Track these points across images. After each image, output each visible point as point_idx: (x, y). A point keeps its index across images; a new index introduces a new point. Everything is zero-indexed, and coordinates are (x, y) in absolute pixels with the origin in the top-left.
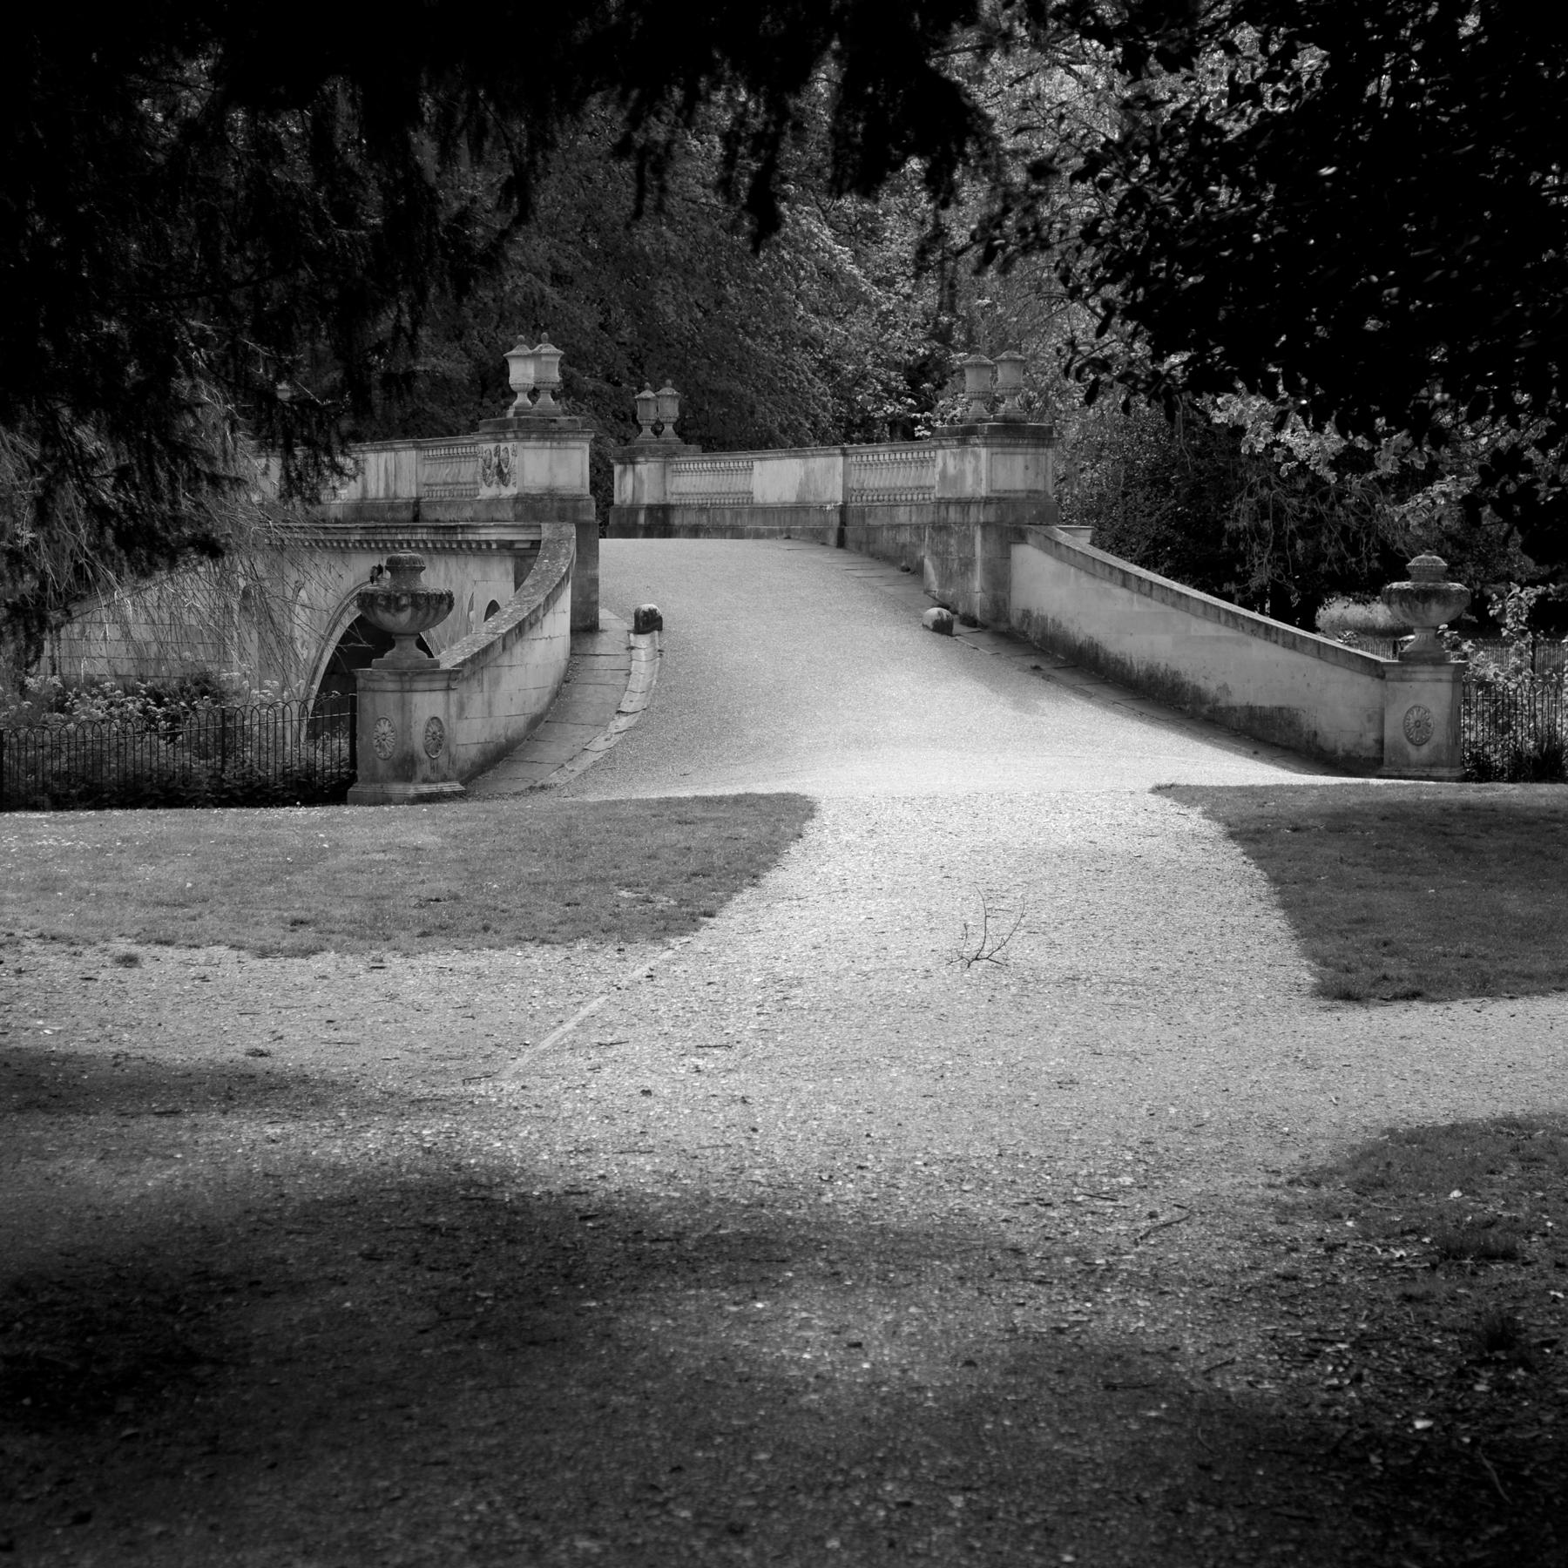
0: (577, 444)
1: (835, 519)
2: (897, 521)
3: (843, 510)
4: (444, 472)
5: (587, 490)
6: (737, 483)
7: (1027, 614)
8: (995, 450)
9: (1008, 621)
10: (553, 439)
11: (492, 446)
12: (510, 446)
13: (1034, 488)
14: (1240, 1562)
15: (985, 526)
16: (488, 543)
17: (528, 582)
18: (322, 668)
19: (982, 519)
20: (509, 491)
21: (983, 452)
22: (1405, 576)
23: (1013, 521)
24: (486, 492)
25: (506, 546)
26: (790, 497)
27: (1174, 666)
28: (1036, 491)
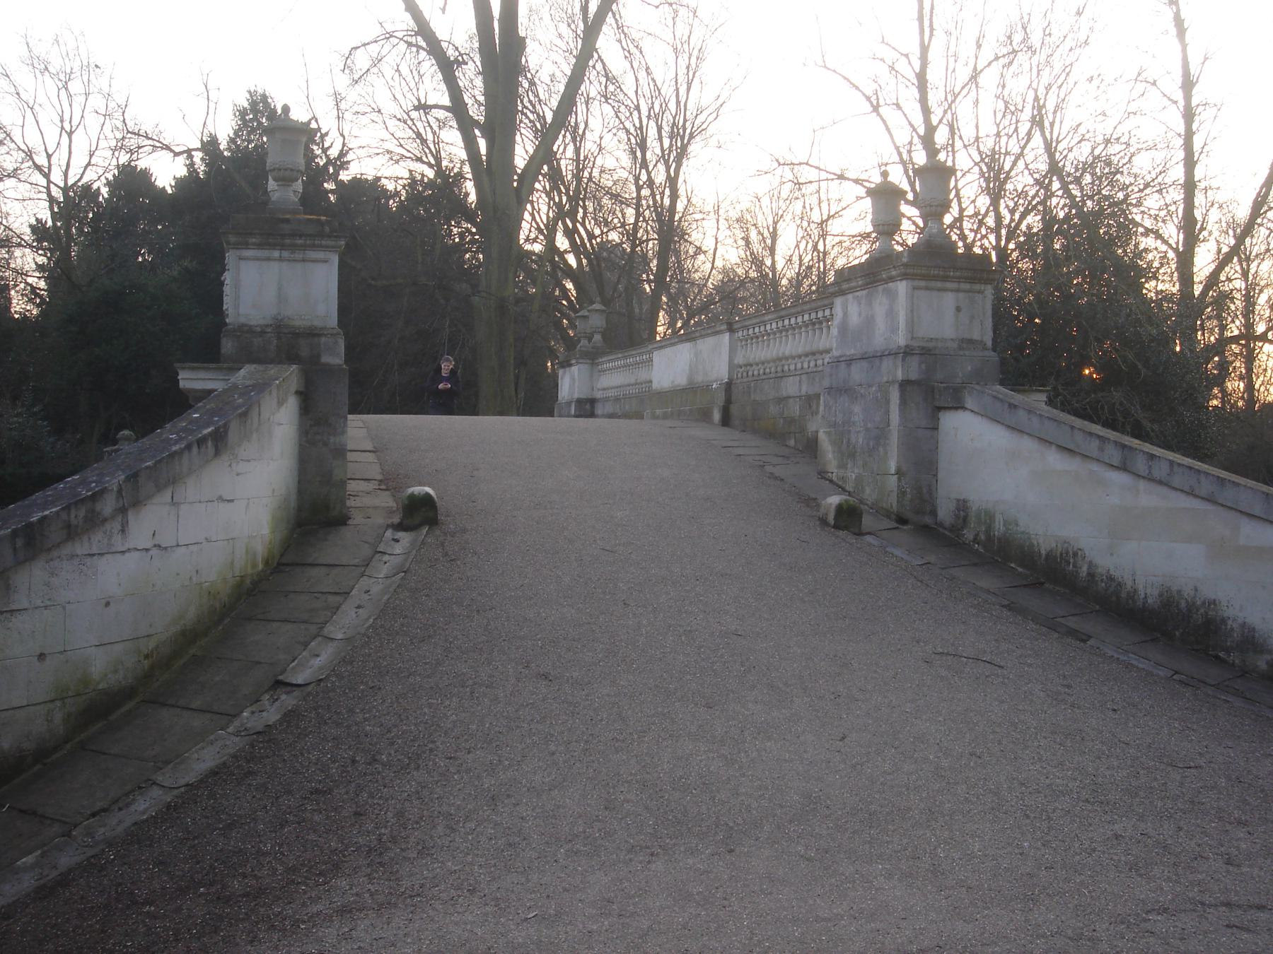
0: (320, 255)
1: (720, 399)
2: (785, 394)
3: (729, 387)
5: (333, 321)
6: (642, 375)
7: (962, 506)
8: (916, 283)
9: (934, 513)
10: (283, 247)
13: (967, 336)
15: (905, 385)
19: (900, 375)
26: (682, 381)
27: (1208, 592)
28: (970, 341)
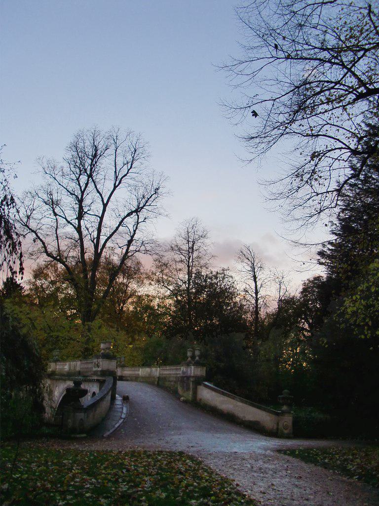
1: (157, 379)
4: (86, 366)
11: (96, 360)
12: (100, 360)
14: (159, 501)
15: (193, 381)
16: (94, 380)
17: (103, 388)
18: (59, 402)
20: (100, 369)
21: (193, 367)
22: (282, 394)
23: (198, 381)
24: (94, 369)
25: (98, 381)
